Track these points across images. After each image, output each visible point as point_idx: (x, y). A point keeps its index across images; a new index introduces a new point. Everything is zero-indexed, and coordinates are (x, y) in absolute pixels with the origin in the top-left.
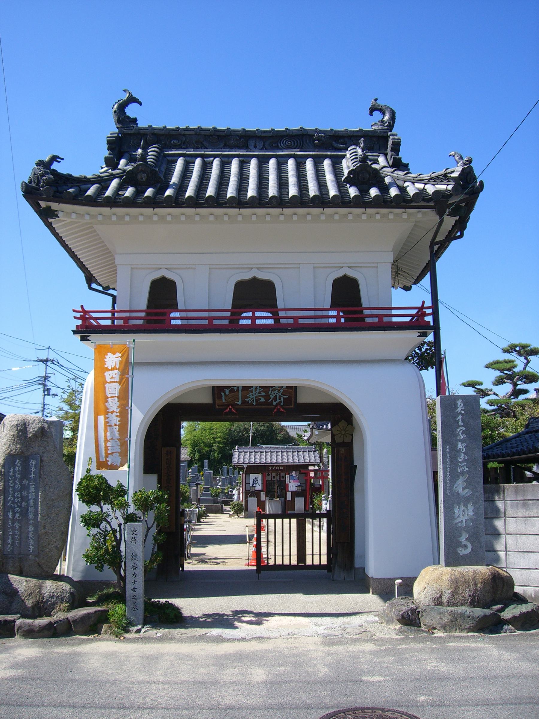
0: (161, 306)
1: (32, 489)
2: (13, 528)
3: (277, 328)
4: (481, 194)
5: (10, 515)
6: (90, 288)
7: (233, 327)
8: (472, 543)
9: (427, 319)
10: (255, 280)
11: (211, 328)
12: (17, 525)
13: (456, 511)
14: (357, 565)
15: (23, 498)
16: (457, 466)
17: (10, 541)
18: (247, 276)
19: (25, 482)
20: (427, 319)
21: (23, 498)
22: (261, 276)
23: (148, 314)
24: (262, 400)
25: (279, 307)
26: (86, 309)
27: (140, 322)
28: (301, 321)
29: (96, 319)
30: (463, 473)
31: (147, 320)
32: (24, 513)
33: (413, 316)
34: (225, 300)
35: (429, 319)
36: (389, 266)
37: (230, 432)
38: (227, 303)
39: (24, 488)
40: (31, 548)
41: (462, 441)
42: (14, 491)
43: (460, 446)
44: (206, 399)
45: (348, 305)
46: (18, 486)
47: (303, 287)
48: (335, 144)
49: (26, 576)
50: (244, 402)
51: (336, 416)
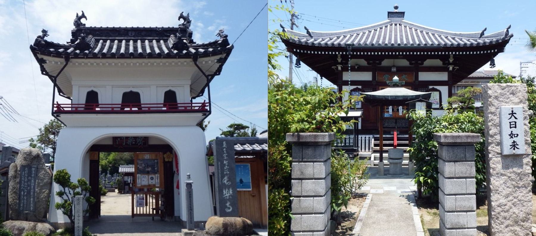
0: (91, 104)
1: (33, 181)
2: (24, 199)
3: (140, 111)
4: (233, 50)
5: (22, 193)
6: (60, 95)
7: (122, 112)
8: (232, 207)
9: (206, 108)
10: (131, 92)
11: (113, 112)
12: (25, 198)
13: (224, 191)
14: (176, 214)
15: (28, 186)
16: (224, 171)
17: (22, 205)
18: (128, 90)
19: (30, 178)
20: (206, 108)
21: (28, 186)
22: (135, 90)
23: (86, 105)
24: (134, 143)
25: (142, 102)
26: (59, 103)
27: (82, 109)
28: (151, 109)
29: (63, 108)
30: (227, 174)
31: (86, 108)
32: (29, 192)
33: (200, 107)
34: (119, 100)
35: (208, 108)
36: (189, 86)
37: (285, 139)
38: (120, 101)
39: (29, 181)
40: (32, 208)
41: (226, 160)
42: (24, 182)
43: (225, 162)
44: (110, 143)
45: (171, 103)
46: (26, 180)
47: (151, 95)
48: (166, 34)
49: (29, 221)
50: (126, 144)
51: (166, 149)
